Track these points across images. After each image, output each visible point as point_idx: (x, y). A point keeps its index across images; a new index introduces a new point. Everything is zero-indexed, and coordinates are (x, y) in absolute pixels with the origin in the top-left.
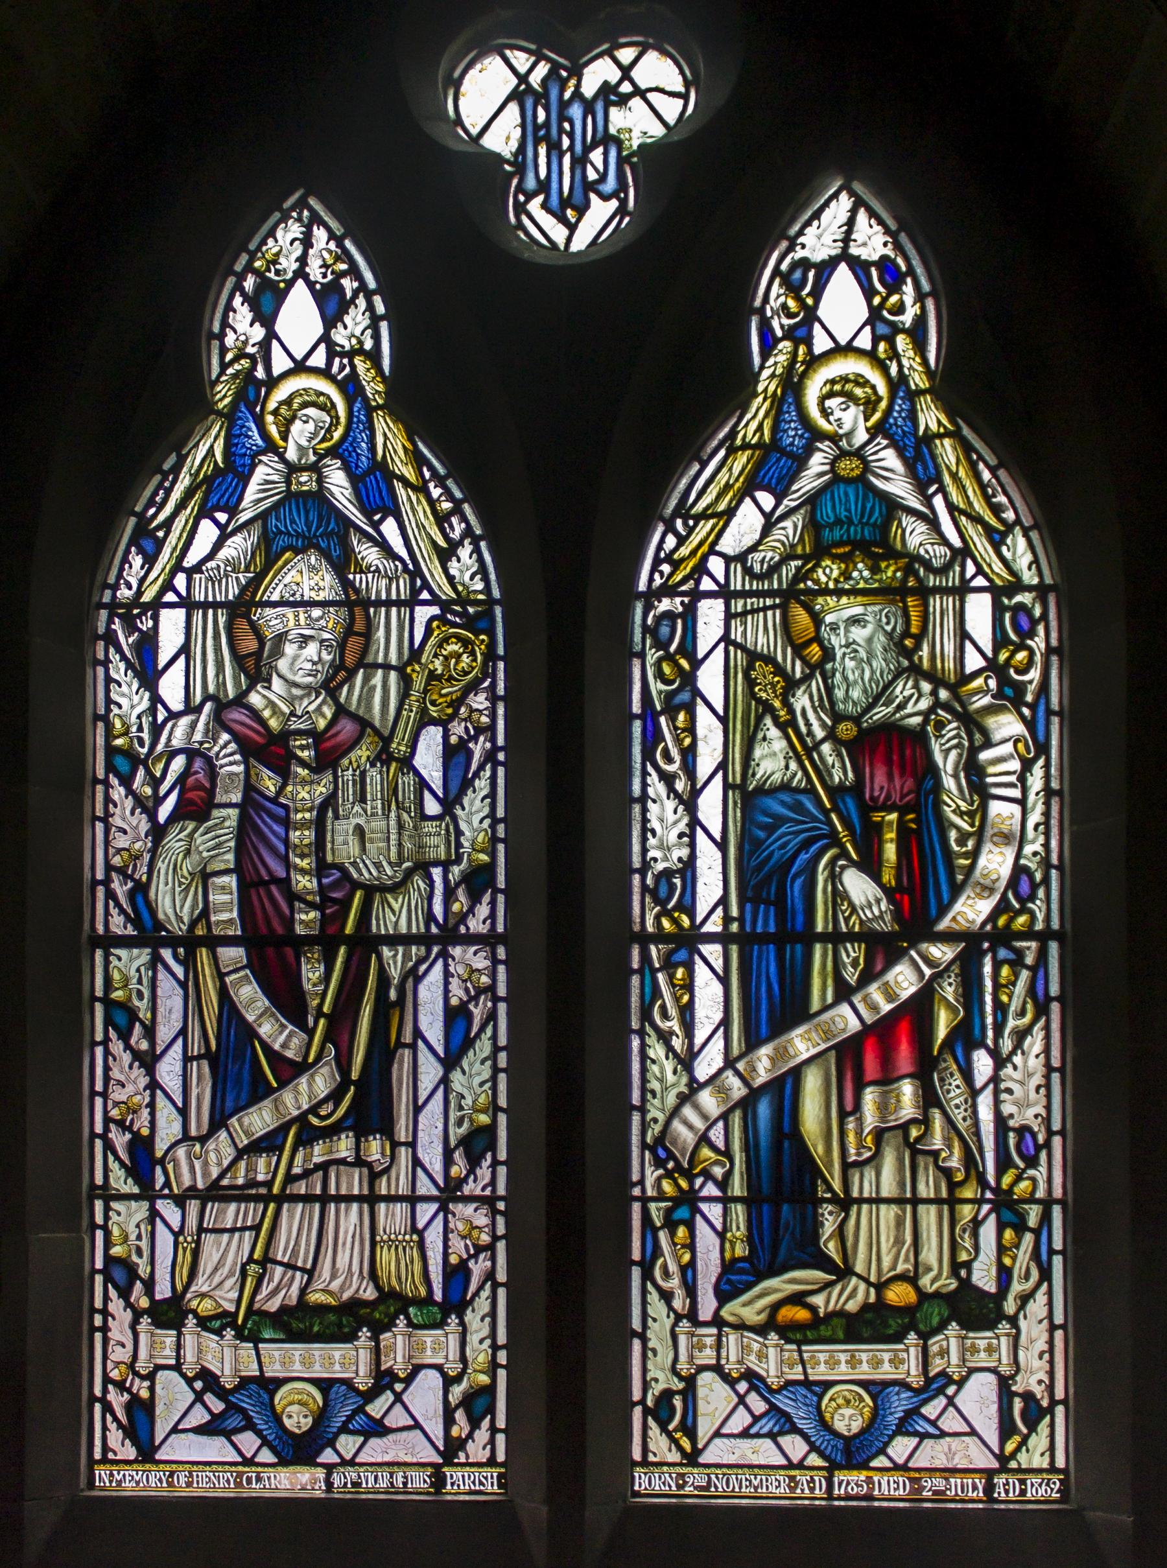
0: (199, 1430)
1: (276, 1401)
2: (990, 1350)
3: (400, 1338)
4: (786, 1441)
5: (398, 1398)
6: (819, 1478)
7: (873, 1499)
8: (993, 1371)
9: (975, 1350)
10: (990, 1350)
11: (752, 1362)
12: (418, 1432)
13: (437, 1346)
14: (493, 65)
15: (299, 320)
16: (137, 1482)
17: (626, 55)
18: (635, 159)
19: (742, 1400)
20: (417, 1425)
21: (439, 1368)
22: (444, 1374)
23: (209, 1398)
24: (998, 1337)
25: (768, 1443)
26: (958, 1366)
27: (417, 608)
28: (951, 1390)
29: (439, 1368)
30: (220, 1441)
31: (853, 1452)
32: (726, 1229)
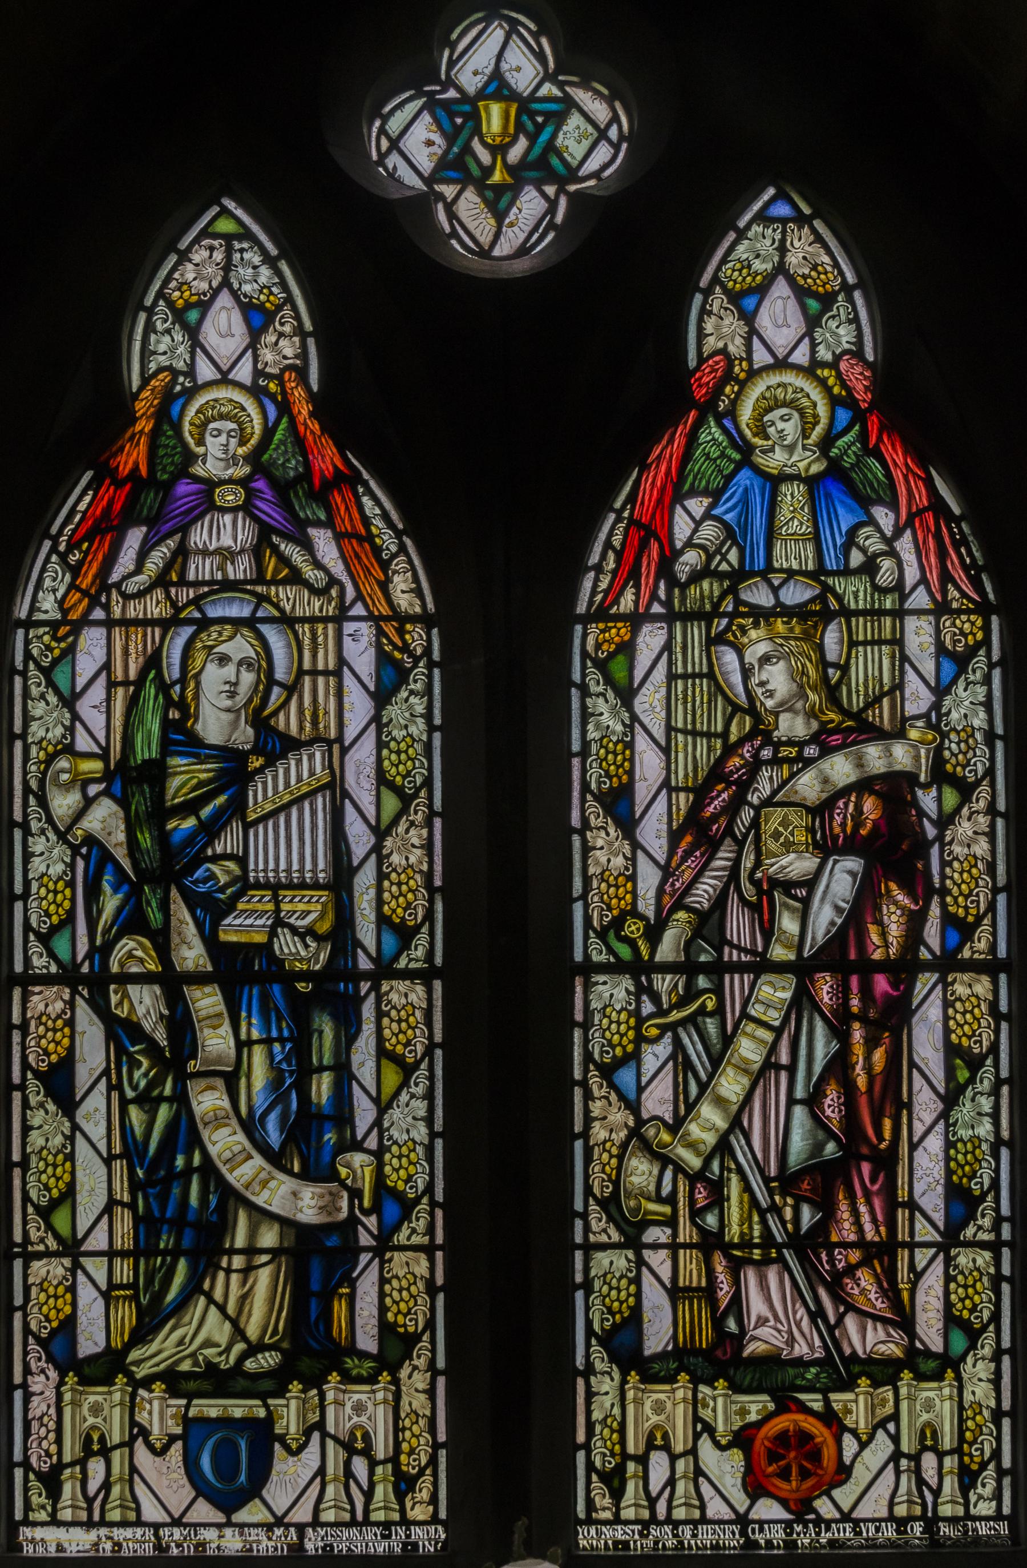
15: (222, 332)
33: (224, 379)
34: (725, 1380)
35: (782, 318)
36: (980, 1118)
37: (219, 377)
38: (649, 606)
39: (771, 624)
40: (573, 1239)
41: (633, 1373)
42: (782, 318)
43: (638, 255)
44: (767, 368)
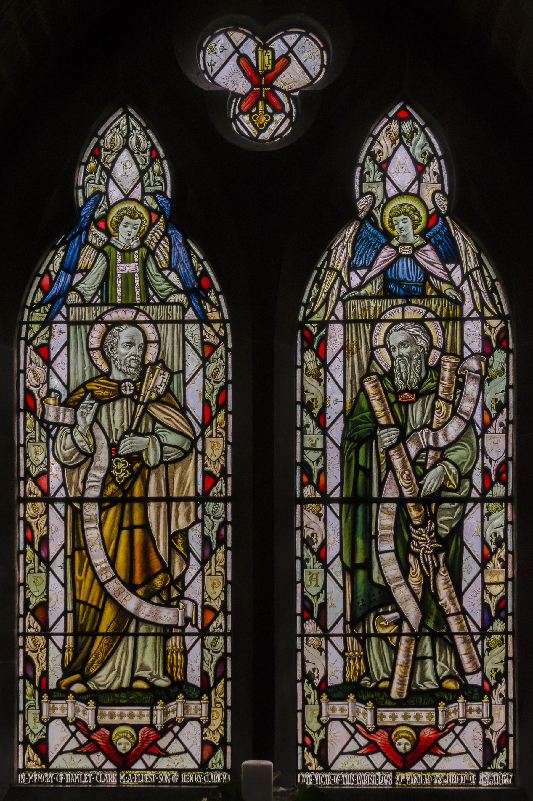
0: (75, 751)
1: (393, 737)
2: (478, 711)
3: (179, 705)
4: (93, 757)
5: (457, 736)
6: (114, 775)
7: (433, 786)
8: (198, 719)
9: (471, 711)
10: (455, 711)
11: (80, 716)
12: (468, 755)
13: (197, 708)
14: (221, 40)
15: (124, 170)
16: (325, 780)
17: (291, 39)
18: (297, 94)
19: (73, 735)
20: (187, 751)
21: (198, 719)
22: (201, 722)
23: (79, 735)
24: (177, 704)
25: (364, 758)
26: (181, 717)
27: (65, 325)
28: (176, 729)
29: (479, 721)
30: (84, 757)
31: (404, 762)
32: (346, 650)
33: (127, 198)
34: (183, 695)
35: (402, 168)
36: (496, 574)
37: (123, 197)
38: (330, 317)
39: (397, 302)
40: (168, 162)
41: (45, 695)
42: (402, 168)
43: (334, 122)
44: (394, 197)
